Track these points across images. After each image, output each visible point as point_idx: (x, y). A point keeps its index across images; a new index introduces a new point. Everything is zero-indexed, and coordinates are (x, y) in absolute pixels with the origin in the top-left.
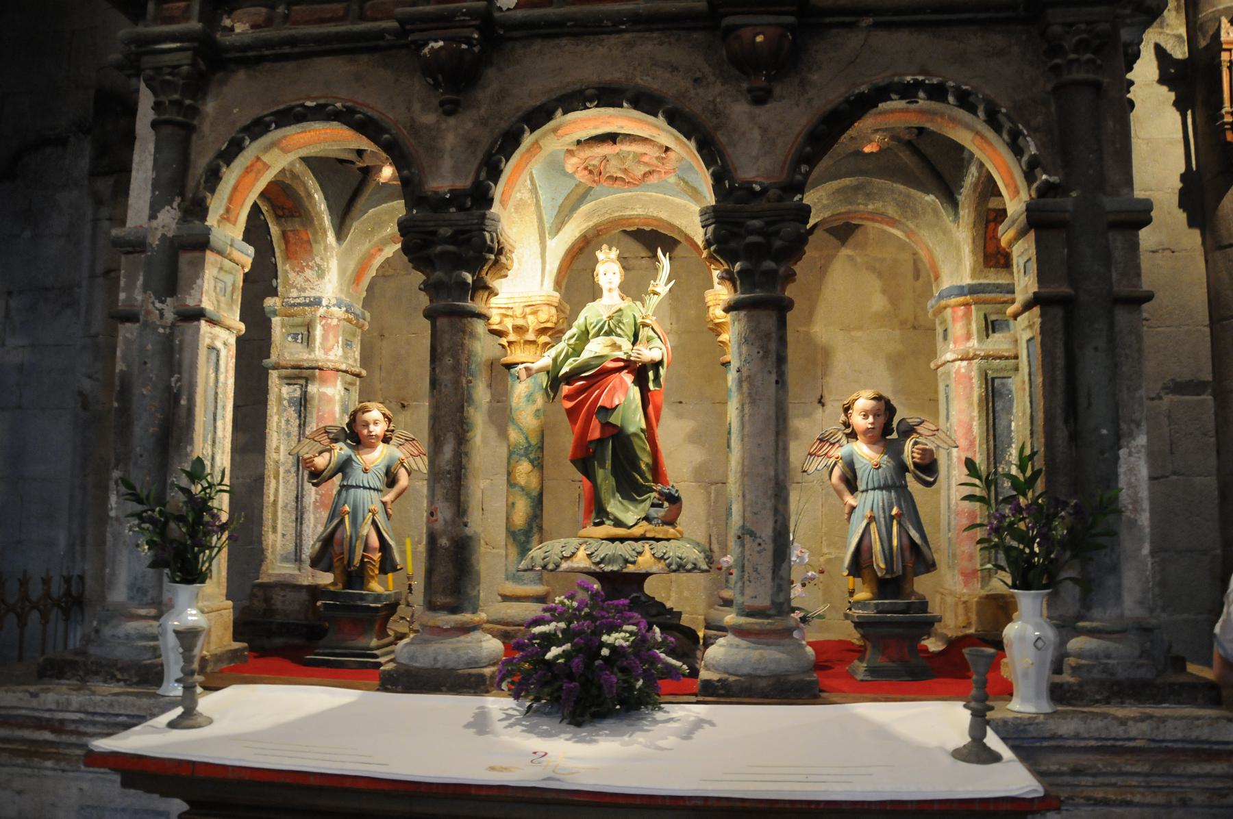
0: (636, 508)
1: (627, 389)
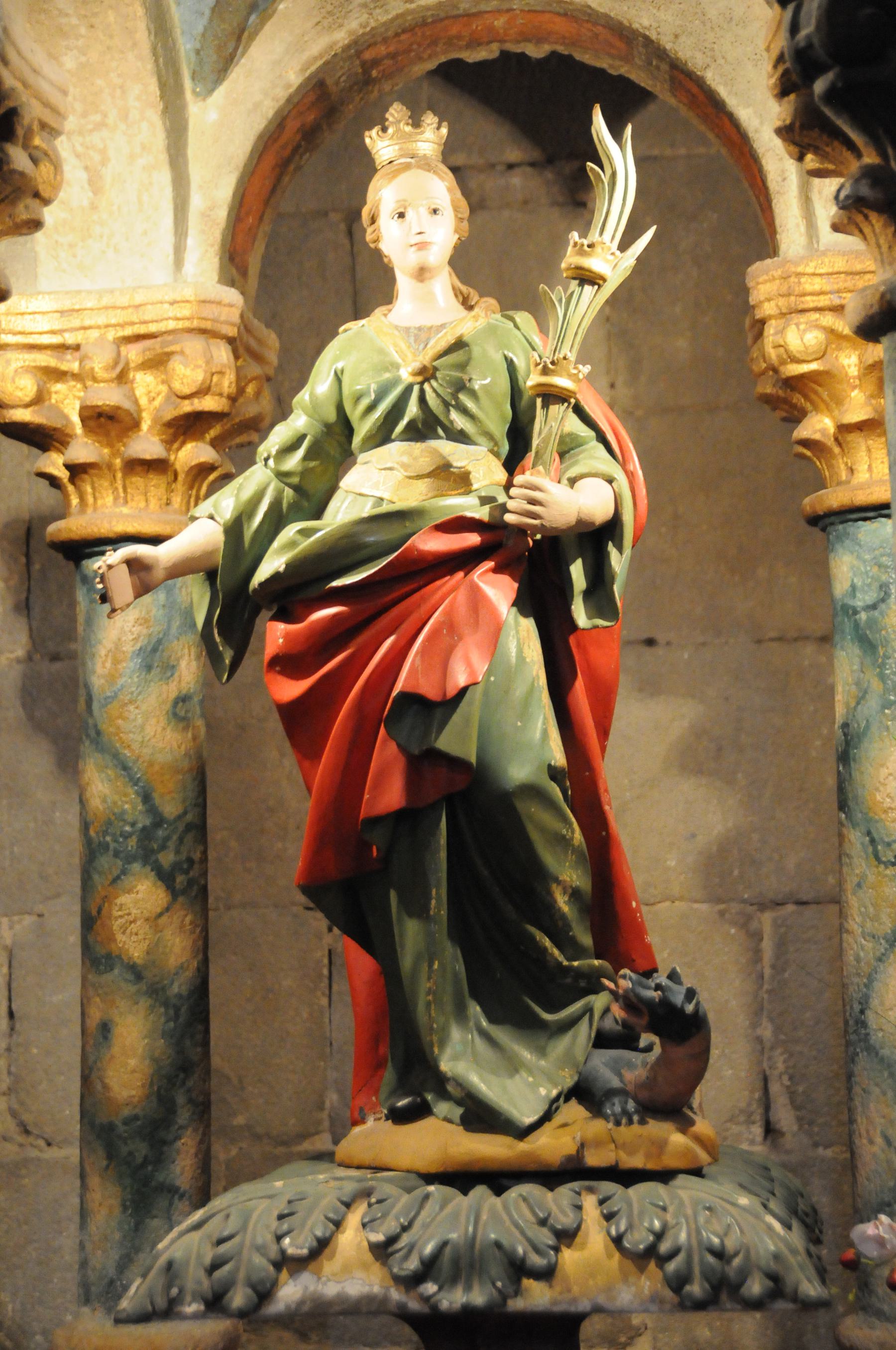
0: (542, 1052)
1: (497, 630)
